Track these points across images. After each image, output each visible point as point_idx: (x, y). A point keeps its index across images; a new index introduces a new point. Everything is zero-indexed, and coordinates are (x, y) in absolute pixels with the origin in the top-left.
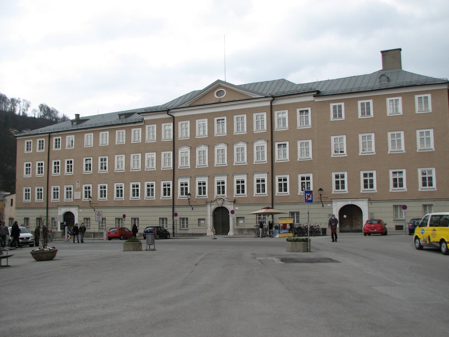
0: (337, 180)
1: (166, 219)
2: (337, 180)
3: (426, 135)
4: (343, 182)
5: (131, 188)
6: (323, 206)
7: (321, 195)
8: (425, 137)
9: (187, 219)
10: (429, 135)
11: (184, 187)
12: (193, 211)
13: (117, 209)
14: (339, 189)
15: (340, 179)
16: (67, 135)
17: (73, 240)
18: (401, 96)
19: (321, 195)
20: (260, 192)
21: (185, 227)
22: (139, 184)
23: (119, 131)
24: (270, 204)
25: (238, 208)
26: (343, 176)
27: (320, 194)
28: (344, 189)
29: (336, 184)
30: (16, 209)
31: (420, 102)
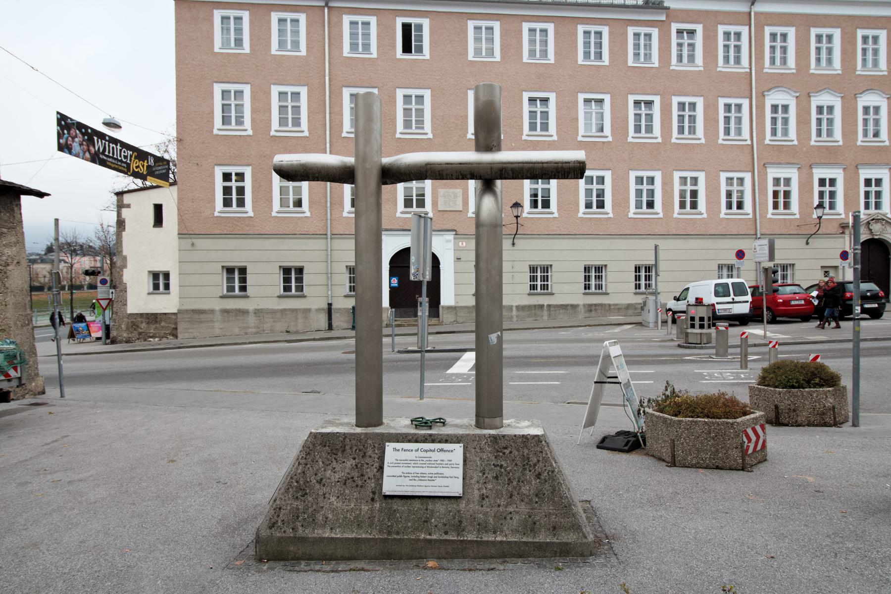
0: (228, 184)
1: (167, 275)
2: (228, 184)
3: (417, 103)
4: (241, 191)
5: (633, 187)
6: (513, 244)
7: (517, 217)
8: (414, 106)
9: (243, 271)
10: (299, 100)
11: (782, 188)
12: (807, 247)
13: (590, 241)
14: (412, 207)
15: (782, 188)
16: (218, 8)
17: (472, 332)
18: (553, 22)
19: (517, 217)
20: (591, 207)
21: (643, 287)
22: (658, 176)
23: (283, 15)
24: (472, 236)
25: (464, 243)
26: (240, 176)
27: (515, 215)
28: (244, 207)
29: (224, 194)
30: (179, 238)
31: (225, 30)
